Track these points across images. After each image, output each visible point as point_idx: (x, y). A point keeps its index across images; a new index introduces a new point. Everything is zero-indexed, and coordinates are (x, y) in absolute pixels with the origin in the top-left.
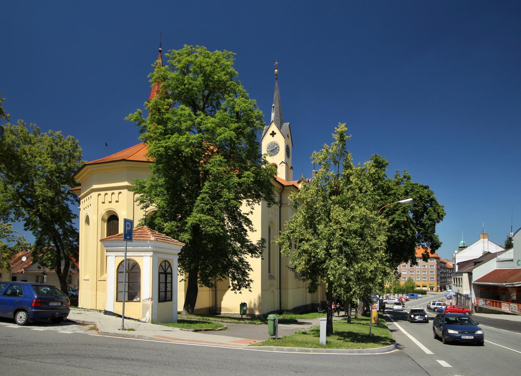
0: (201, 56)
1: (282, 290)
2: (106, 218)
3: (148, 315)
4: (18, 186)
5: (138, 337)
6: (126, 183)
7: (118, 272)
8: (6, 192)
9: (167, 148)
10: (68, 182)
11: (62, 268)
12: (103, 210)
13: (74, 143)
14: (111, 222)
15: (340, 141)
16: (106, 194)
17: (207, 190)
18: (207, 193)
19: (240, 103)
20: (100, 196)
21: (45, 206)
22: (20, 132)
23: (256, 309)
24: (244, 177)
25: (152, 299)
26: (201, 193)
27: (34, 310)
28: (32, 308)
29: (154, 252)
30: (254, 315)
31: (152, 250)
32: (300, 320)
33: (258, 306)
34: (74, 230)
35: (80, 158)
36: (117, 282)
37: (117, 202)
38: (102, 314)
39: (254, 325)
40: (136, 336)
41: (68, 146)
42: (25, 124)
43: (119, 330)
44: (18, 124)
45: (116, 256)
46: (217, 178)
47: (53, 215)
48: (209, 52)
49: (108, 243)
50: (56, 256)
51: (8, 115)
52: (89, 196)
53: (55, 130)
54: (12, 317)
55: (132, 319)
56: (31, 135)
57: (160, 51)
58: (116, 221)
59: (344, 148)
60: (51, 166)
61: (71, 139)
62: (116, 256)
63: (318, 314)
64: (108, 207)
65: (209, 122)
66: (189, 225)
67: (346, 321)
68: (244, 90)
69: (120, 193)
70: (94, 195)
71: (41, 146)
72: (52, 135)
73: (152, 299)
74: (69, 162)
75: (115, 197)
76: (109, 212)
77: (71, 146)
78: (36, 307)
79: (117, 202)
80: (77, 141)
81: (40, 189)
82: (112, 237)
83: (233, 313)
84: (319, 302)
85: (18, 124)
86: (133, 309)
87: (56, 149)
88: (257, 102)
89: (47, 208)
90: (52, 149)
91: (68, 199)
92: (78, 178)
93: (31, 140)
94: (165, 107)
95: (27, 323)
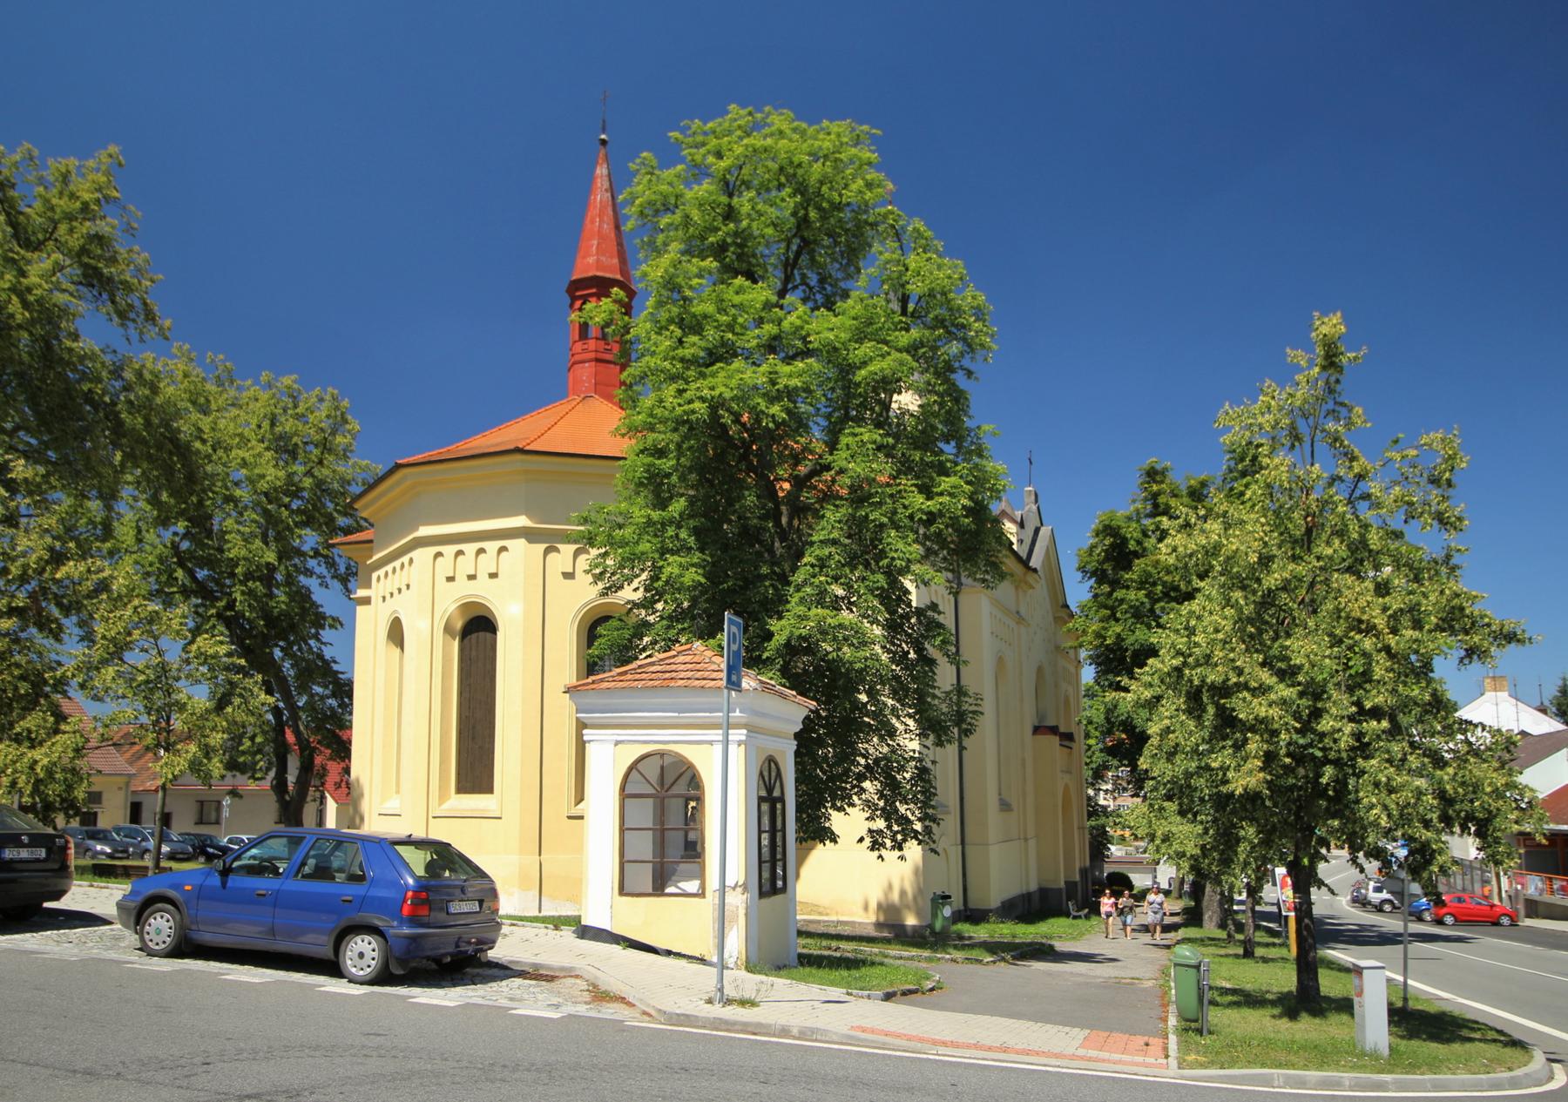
0: (785, 135)
1: (968, 848)
2: (459, 624)
3: (736, 943)
4: (175, 534)
5: (803, 1035)
6: (521, 521)
7: (625, 795)
8: (141, 550)
9: (715, 405)
10: (329, 522)
11: (291, 778)
12: (450, 601)
13: (337, 408)
14: (474, 636)
15: (1324, 368)
16: (460, 553)
17: (835, 535)
18: (834, 542)
19: (931, 269)
20: (440, 559)
21: (250, 593)
22: (180, 377)
23: (908, 907)
24: (941, 494)
25: (745, 887)
26: (812, 544)
27: (406, 931)
28: (402, 923)
29: (752, 729)
30: (903, 927)
31: (744, 721)
32: (1060, 946)
33: (915, 898)
34: (327, 663)
35: (345, 455)
36: (622, 830)
37: (493, 576)
38: (567, 933)
39: (978, 966)
40: (795, 1032)
41: (321, 414)
42: (193, 355)
43: (710, 1001)
44: (175, 356)
45: (617, 743)
46: (860, 495)
47: (271, 620)
48: (804, 125)
49: (590, 699)
50: (275, 741)
51: (167, 323)
52: (405, 559)
53: (279, 373)
54: (326, 952)
55: (679, 955)
56: (211, 387)
57: (604, 142)
58: (489, 635)
59: (1331, 391)
60: (273, 474)
61: (328, 397)
62: (617, 743)
63: (1069, 921)
64: (464, 591)
65: (826, 327)
66: (779, 639)
67: (1241, 951)
68: (929, 234)
69: (503, 549)
70: (423, 555)
71: (241, 420)
72: (269, 386)
73: (745, 887)
74: (320, 462)
75: (487, 563)
76: (466, 607)
77: (328, 417)
78: (414, 920)
79: (493, 576)
80: (346, 403)
81: (241, 541)
82: (602, 680)
83: (834, 918)
84: (1062, 885)
85: (175, 356)
86: (679, 919)
87: (288, 425)
88: (966, 267)
89: (256, 598)
90: (273, 424)
91: (309, 573)
92: (366, 507)
93: (208, 401)
94: (695, 281)
95: (384, 977)
